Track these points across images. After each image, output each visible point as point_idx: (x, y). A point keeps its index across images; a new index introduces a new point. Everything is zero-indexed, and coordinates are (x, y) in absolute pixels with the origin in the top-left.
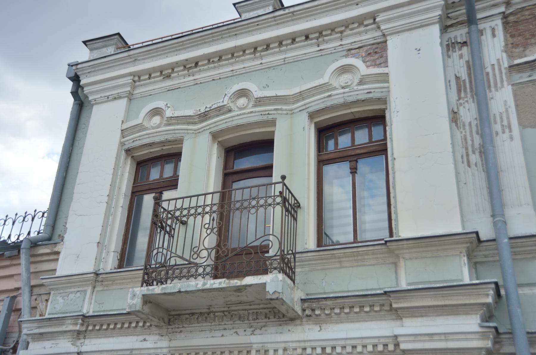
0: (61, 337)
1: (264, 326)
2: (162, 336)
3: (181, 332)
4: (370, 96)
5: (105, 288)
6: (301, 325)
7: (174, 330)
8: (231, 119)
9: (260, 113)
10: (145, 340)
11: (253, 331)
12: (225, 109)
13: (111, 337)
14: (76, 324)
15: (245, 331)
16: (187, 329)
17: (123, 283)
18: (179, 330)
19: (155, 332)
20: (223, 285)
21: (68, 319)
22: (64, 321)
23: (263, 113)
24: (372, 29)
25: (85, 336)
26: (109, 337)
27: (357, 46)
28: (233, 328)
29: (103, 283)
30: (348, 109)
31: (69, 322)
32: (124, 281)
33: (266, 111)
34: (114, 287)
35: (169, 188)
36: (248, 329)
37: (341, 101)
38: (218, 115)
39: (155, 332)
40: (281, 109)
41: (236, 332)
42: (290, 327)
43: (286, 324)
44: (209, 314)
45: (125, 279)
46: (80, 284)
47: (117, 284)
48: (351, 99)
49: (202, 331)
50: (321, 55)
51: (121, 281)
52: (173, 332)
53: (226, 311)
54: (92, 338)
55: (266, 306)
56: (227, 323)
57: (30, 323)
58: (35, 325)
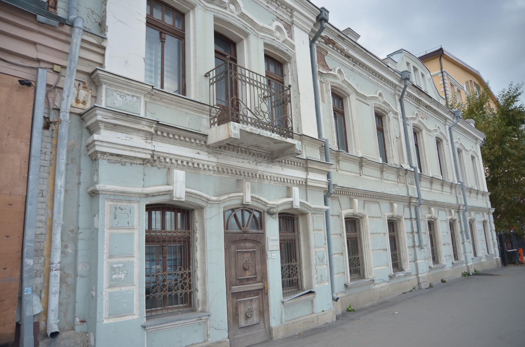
0: (134, 134)
1: (261, 162)
2: (210, 154)
3: (220, 154)
4: (287, 52)
5: (152, 101)
6: (275, 165)
7: (216, 151)
8: (227, 15)
9: (243, 24)
10: (198, 153)
11: (256, 163)
12: (224, 5)
13: (174, 144)
14: (151, 127)
15: (253, 162)
16: (225, 153)
17: (168, 103)
18: (219, 152)
19: (205, 150)
20: (276, 138)
21: (145, 121)
22: (142, 121)
23: (244, 25)
24: (289, 15)
25: (152, 138)
26: (172, 144)
27: (281, 18)
28: (247, 159)
29: (153, 97)
30: (274, 51)
31: (145, 123)
32: (170, 102)
33: (246, 25)
34: (160, 103)
35: (172, 35)
36: (254, 162)
37: (277, 46)
38: (218, 6)
39: (205, 150)
40: (254, 31)
41: (249, 162)
42: (271, 165)
43: (270, 164)
44: (238, 147)
45: (172, 101)
46: (136, 90)
47: (163, 101)
48: (281, 48)
49: (232, 156)
50: (267, 10)
51: (167, 101)
52: (216, 153)
53: (247, 149)
54: (159, 141)
55: (264, 151)
56: (245, 155)
57: (105, 112)
58: (110, 115)
